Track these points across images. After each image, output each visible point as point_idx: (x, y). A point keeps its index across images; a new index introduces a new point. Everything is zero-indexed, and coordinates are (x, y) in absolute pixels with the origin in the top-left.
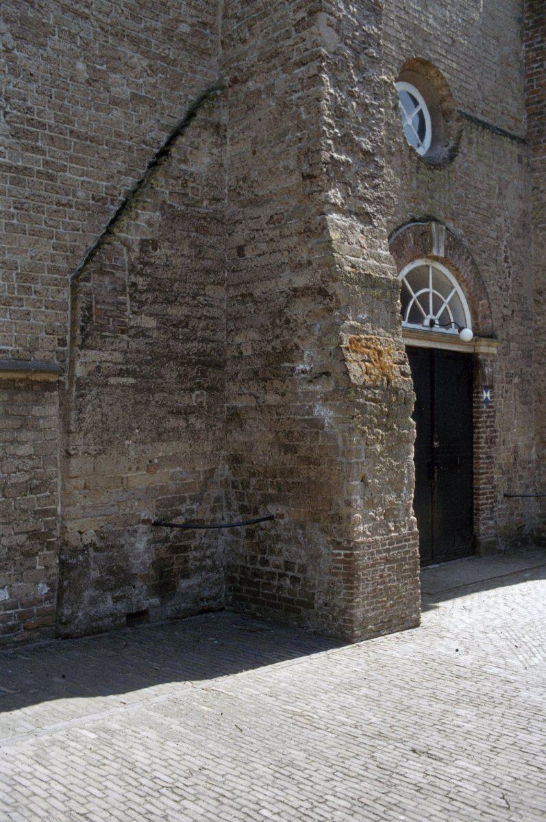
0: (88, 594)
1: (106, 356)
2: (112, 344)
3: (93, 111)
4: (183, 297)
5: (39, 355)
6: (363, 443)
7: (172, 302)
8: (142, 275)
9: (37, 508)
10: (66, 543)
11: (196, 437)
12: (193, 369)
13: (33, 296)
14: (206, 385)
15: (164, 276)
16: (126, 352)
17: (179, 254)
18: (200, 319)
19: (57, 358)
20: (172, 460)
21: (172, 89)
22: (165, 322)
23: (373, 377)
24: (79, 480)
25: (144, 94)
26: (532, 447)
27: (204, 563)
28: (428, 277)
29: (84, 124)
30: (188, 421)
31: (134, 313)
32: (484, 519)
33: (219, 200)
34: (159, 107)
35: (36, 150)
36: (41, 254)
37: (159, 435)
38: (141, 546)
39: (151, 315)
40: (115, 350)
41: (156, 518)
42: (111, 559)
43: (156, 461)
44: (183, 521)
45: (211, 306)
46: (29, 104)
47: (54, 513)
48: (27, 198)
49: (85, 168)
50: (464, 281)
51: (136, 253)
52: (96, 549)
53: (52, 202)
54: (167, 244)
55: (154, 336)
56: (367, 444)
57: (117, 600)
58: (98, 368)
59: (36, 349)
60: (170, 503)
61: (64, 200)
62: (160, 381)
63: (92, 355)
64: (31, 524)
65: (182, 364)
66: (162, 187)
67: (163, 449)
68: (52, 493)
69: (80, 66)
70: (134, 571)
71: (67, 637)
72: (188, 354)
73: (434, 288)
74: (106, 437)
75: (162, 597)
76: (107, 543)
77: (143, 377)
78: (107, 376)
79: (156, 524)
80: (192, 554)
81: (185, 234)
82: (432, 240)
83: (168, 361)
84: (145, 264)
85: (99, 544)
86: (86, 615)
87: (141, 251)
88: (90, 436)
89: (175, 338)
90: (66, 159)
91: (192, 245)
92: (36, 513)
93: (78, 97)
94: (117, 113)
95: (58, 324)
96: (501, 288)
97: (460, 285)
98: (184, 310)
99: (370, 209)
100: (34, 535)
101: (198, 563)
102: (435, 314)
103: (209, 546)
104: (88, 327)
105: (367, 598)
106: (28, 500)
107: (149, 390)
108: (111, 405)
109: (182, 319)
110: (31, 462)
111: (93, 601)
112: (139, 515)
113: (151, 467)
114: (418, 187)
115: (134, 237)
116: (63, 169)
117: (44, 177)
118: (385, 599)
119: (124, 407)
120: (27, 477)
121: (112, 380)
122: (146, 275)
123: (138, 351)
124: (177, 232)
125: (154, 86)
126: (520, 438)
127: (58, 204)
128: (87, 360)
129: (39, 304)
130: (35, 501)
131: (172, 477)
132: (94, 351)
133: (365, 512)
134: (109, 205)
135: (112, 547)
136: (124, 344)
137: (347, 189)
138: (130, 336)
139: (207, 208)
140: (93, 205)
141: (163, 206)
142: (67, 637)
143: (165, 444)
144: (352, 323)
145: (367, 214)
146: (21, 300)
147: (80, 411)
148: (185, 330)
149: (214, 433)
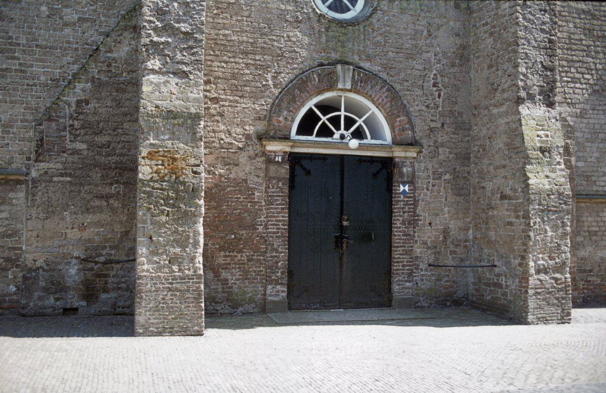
0: (36, 295)
1: (51, 165)
2: (56, 159)
3: (51, 32)
4: (106, 130)
5: (14, 166)
6: (149, 215)
7: (98, 134)
8: (77, 120)
9: (10, 246)
10: (26, 266)
11: (114, 212)
12: (113, 172)
13: (11, 135)
14: (122, 181)
15: (93, 119)
16: (65, 163)
17: (104, 106)
18: (118, 142)
19: (25, 167)
20: (99, 224)
21: (108, 10)
22: (91, 145)
23: (161, 175)
24: (34, 232)
25: (87, 16)
26: (468, 229)
27: (120, 286)
28: (341, 102)
29: (45, 40)
30: (108, 202)
31: (71, 141)
32: (399, 280)
33: (134, 71)
34: (98, 22)
35: (14, 58)
36: (16, 113)
37: (88, 209)
38: (73, 271)
39: (83, 142)
40: (58, 162)
41: (85, 257)
42: (52, 276)
43: (85, 224)
44: (104, 259)
45: (127, 134)
46: (10, 34)
47: (20, 249)
48: (8, 84)
49: (45, 64)
50: (379, 104)
51: (74, 107)
52: (44, 270)
53: (24, 85)
54: (95, 101)
55: (85, 153)
56: (152, 216)
57: (57, 299)
58: (46, 173)
59: (13, 163)
60: (95, 248)
61: (31, 82)
62: (88, 179)
63: (43, 165)
64: (6, 254)
65: (105, 169)
66: (92, 68)
67: (90, 218)
68: (19, 238)
69: (44, 8)
70: (67, 285)
71: (23, 315)
72: (109, 163)
73: (324, 115)
74: (50, 209)
75: (88, 302)
76: (51, 267)
77: (77, 177)
78: (52, 177)
79: (85, 260)
80: (110, 280)
81: (108, 94)
82: (338, 78)
83: (95, 168)
84: (80, 113)
85: (46, 268)
86: (35, 305)
87: (77, 106)
88: (40, 208)
89: (101, 155)
90: (33, 61)
91: (114, 100)
92: (9, 248)
93: (42, 25)
94: (67, 31)
95: (26, 149)
96: (428, 107)
97: (377, 107)
98: (107, 138)
99: (185, 69)
100: (8, 260)
101: (115, 285)
102: (347, 129)
103: (123, 276)
104: (41, 150)
105: (150, 310)
106: (6, 241)
107: (81, 184)
108: (54, 192)
109: (105, 143)
110: (7, 222)
111: (40, 298)
112: (73, 254)
113: (82, 228)
114: (327, 41)
115: (72, 99)
116: (32, 66)
117: (19, 72)
118: (167, 313)
119: (63, 193)
120: (5, 229)
121: (55, 179)
122: (80, 120)
123: (73, 163)
124: (103, 93)
125: (95, 11)
126: (452, 222)
127: (28, 85)
128: (39, 168)
129: (14, 139)
130: (9, 242)
131: (98, 234)
132: (44, 163)
133: (150, 257)
134: (62, 83)
135: (54, 270)
136: (64, 159)
137: (166, 59)
138: (68, 154)
139: (126, 77)
140: (51, 83)
141: (93, 80)
142: (23, 315)
143: (91, 215)
144: (152, 141)
145: (184, 72)
146: (4, 137)
147: (34, 195)
148: (108, 149)
149: (128, 210)
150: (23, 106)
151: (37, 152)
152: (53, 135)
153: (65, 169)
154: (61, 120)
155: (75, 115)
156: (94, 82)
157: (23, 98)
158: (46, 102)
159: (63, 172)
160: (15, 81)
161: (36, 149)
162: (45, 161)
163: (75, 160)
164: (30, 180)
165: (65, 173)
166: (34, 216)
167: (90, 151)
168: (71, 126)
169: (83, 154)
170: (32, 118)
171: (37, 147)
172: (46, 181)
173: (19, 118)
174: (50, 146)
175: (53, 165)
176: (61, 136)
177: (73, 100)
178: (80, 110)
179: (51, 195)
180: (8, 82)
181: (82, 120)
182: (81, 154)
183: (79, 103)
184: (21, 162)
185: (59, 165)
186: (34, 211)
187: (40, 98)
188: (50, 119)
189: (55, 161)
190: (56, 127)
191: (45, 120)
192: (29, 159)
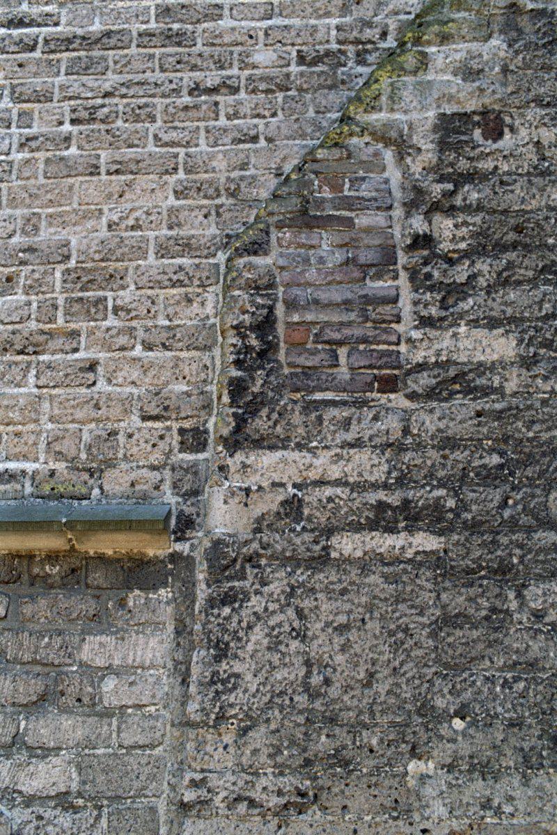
1: (321, 464)
2: (346, 424)
5: (116, 481)
8: (451, 211)
16: (400, 448)
31: (425, 322)
39: (493, 324)
40: (357, 444)
48: (107, 95)
51: (429, 155)
54: (534, 113)
55: (511, 386)
58: (293, 508)
59: (110, 464)
61: (212, 78)
74: (323, 744)
77: (474, 527)
78: (329, 532)
87: (443, 146)
88: (258, 737)
104: (262, 381)
107: (503, 571)
108: (342, 629)
115: (415, 116)
119: (399, 636)
121: (347, 545)
122: (467, 209)
123: (448, 443)
127: (196, 90)
128: (252, 481)
129: (123, 340)
136: (392, 424)
138: (412, 396)
146: (75, 334)
147: (222, 652)
150: (172, 179)
151: (237, 388)
152: (323, 296)
153: (402, 482)
154: (362, 220)
155: (437, 189)
156: (520, 31)
157: (173, 144)
158: (279, 155)
159: (394, 499)
160: (140, 77)
161: (235, 373)
162: (280, 443)
163: (454, 429)
164: (198, 555)
165: (406, 502)
166: (224, 785)
167: (540, 369)
168: (422, 241)
169: (500, 391)
170: (213, 230)
171: (238, 363)
172: (291, 561)
173: (151, 234)
174: (314, 353)
175: (328, 463)
176: (368, 300)
177: (417, 115)
178: (463, 165)
179: (322, 645)
180: (107, 86)
181: (479, 208)
182: (486, 391)
183: (452, 129)
184: (156, 457)
185: (362, 458)
186: (220, 757)
187: (255, 139)
188: (306, 218)
189: (342, 436)
190: (339, 257)
191: (280, 226)
192: (195, 439)
